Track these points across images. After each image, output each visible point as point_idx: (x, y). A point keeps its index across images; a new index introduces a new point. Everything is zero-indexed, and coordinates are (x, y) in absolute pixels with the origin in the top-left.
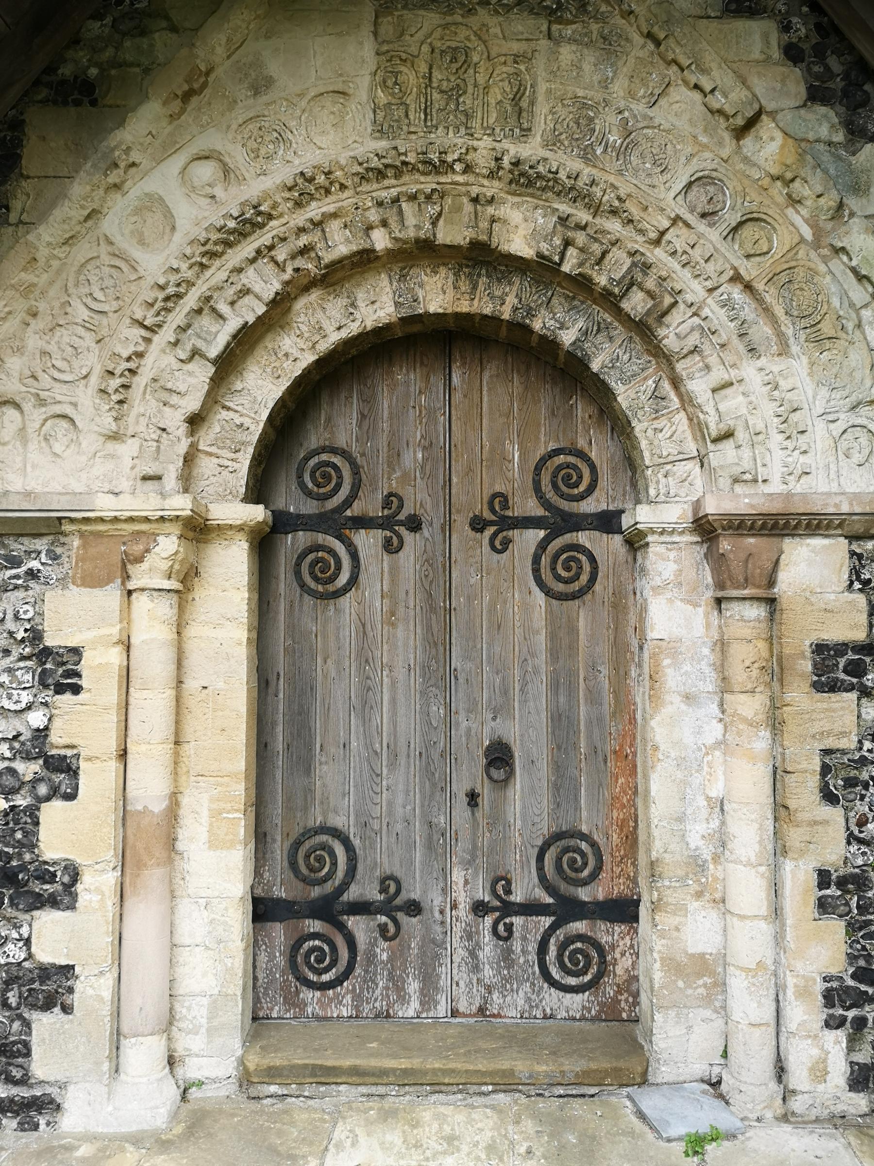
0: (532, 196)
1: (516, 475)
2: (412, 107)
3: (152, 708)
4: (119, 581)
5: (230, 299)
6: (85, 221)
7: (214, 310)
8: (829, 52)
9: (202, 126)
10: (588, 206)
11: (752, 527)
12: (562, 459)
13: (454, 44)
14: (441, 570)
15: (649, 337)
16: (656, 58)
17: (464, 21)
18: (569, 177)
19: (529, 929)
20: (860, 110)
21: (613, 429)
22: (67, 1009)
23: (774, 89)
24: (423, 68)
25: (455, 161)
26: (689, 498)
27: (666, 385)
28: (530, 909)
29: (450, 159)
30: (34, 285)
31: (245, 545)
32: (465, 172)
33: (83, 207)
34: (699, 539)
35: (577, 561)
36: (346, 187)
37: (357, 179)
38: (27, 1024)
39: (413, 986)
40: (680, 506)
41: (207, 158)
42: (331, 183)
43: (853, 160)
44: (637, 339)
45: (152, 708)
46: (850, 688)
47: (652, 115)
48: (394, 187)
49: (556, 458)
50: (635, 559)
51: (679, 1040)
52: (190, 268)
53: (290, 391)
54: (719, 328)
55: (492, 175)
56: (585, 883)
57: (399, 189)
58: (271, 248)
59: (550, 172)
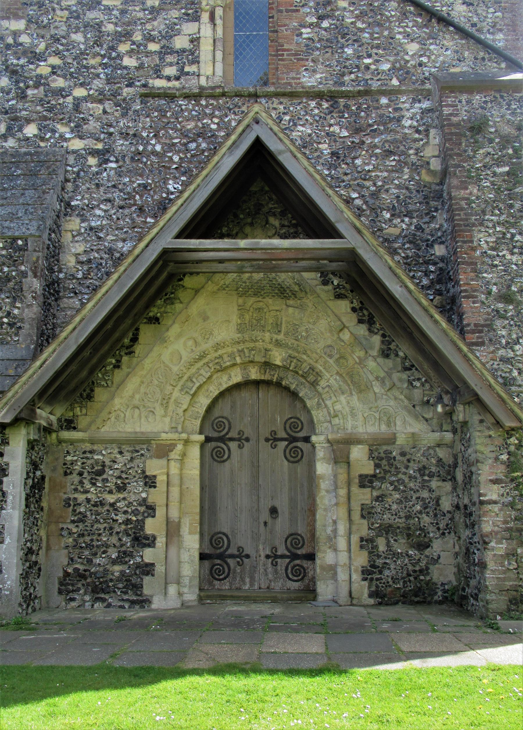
3: (175, 491)
12: (292, 420)
19: (282, 563)
22: (153, 575)
28: (282, 557)
38: (142, 579)
39: (247, 580)
45: (175, 491)
46: (369, 487)
51: (325, 590)
56: (299, 549)
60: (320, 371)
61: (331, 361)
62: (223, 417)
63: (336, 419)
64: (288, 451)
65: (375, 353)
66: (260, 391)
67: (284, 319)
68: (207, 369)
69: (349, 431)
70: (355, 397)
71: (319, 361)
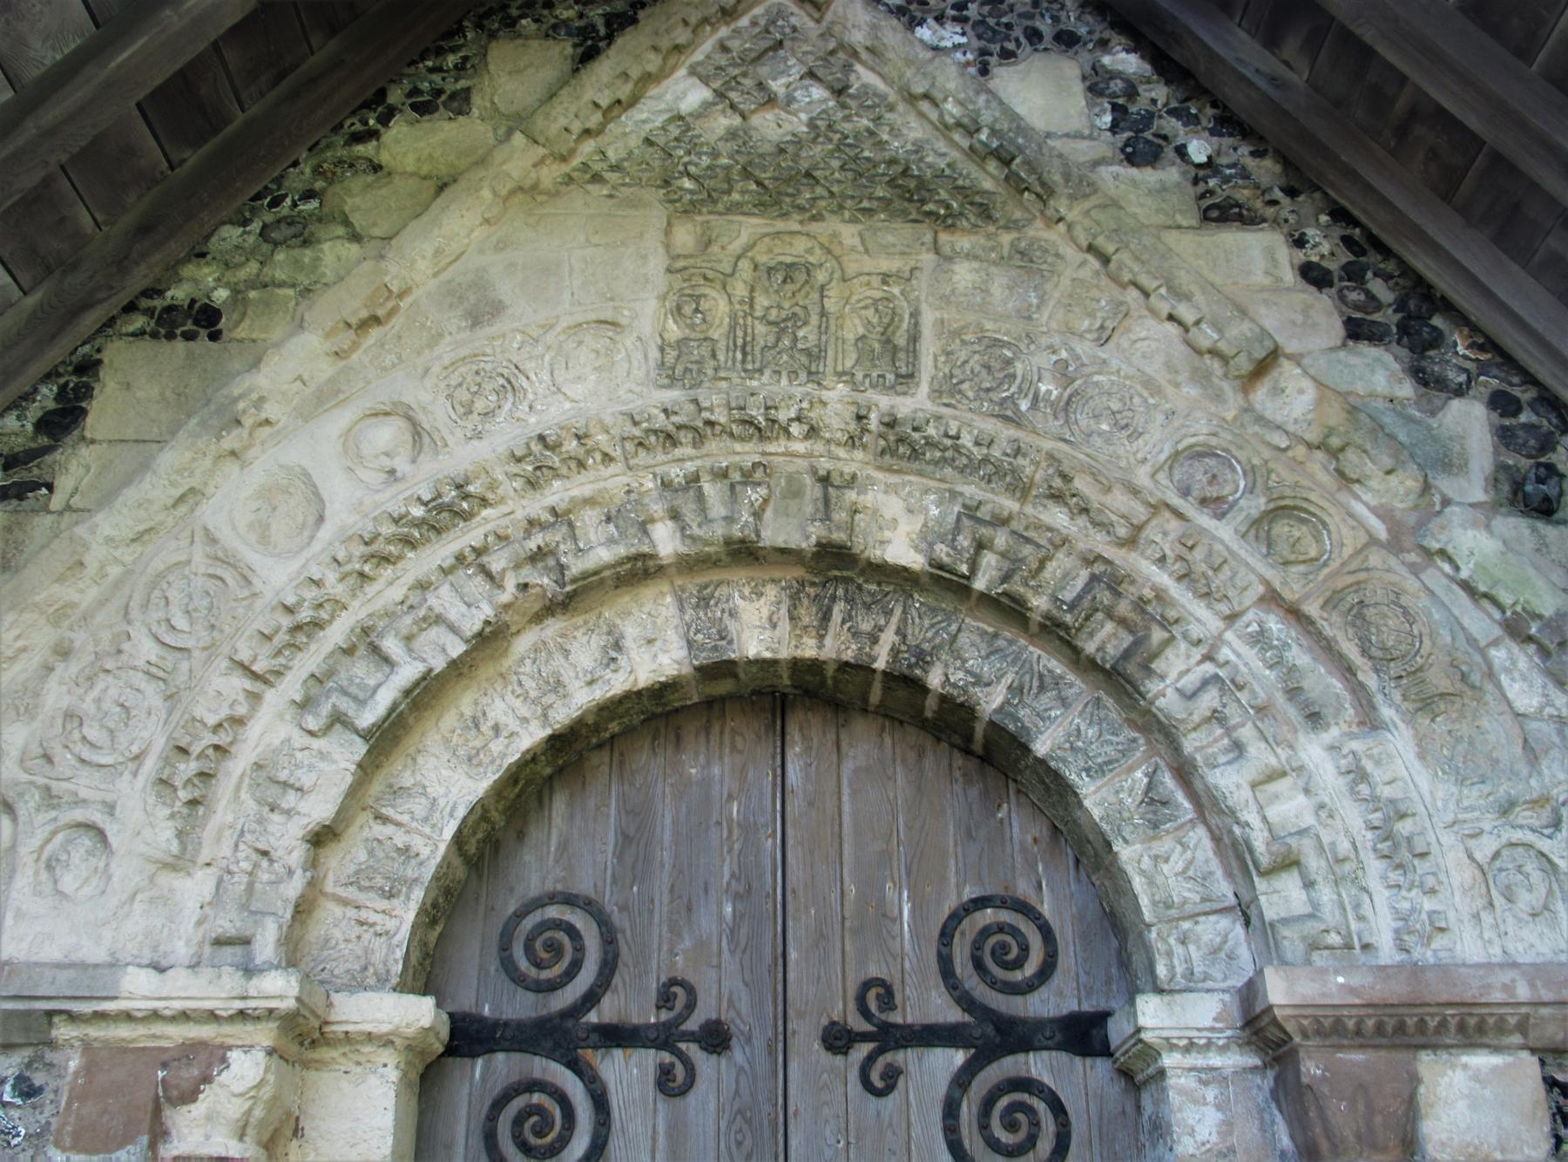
0: (920, 473)
1: (907, 946)
2: (722, 345)
4: (145, 1139)
5: (404, 632)
6: (174, 506)
7: (375, 649)
8: (1369, 275)
9: (384, 369)
10: (1011, 489)
11: (1358, 1032)
12: (989, 915)
13: (788, 260)
14: (767, 1133)
15: (1130, 696)
16: (1104, 281)
17: (805, 229)
18: (977, 444)
20: (1432, 353)
21: (1077, 862)
23: (1294, 323)
24: (740, 290)
25: (791, 420)
26: (1229, 983)
27: (1168, 781)
29: (782, 416)
30: (72, 605)
31: (393, 1075)
32: (807, 437)
33: (173, 484)
34: (1258, 1062)
35: (1030, 1111)
36: (611, 459)
37: (630, 446)
40: (1217, 997)
41: (387, 414)
42: (588, 452)
43: (1434, 423)
44: (1109, 702)
47: (1104, 356)
48: (691, 459)
49: (978, 914)
50: (1138, 1108)
52: (342, 580)
53: (498, 791)
54: (1249, 678)
55: (852, 442)
57: (699, 463)
58: (479, 552)
59: (946, 435)
60: (1160, 596)
61: (1225, 532)
62: (570, 900)
63: (1289, 884)
64: (968, 1111)
65: (1473, 487)
66: (795, 751)
67: (928, 318)
68: (478, 585)
69: (1387, 953)
70: (1400, 742)
71: (1151, 532)
